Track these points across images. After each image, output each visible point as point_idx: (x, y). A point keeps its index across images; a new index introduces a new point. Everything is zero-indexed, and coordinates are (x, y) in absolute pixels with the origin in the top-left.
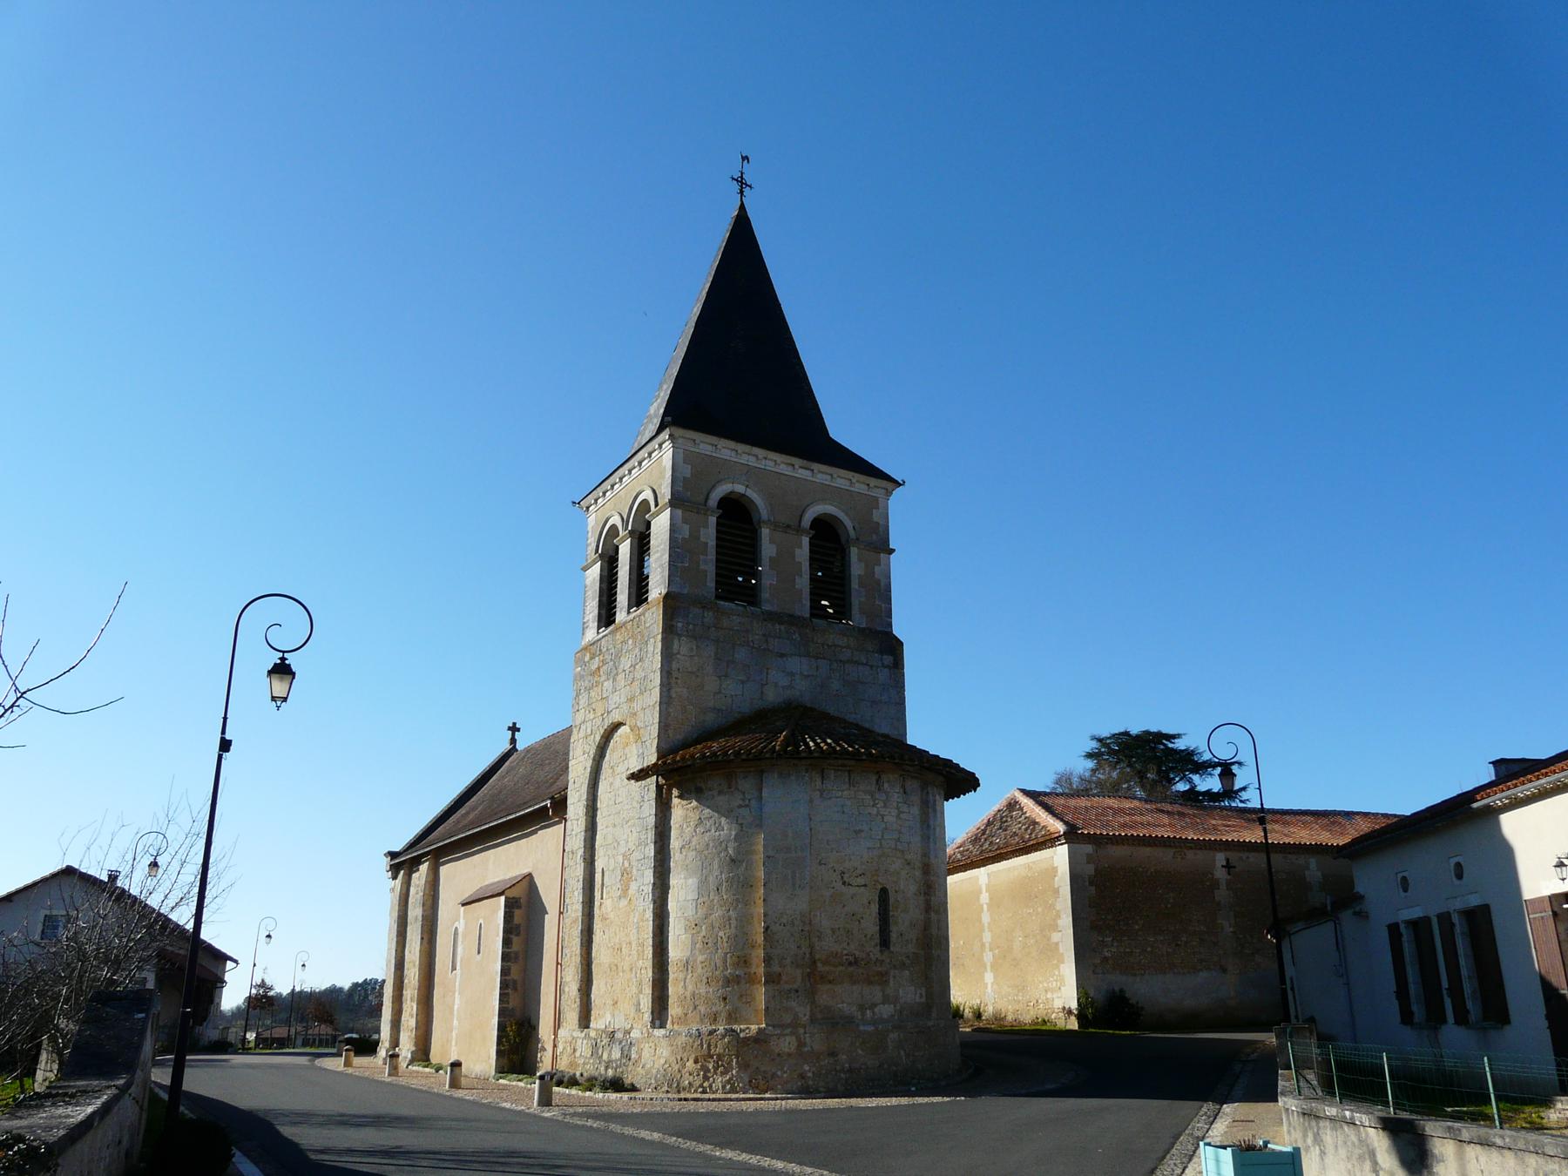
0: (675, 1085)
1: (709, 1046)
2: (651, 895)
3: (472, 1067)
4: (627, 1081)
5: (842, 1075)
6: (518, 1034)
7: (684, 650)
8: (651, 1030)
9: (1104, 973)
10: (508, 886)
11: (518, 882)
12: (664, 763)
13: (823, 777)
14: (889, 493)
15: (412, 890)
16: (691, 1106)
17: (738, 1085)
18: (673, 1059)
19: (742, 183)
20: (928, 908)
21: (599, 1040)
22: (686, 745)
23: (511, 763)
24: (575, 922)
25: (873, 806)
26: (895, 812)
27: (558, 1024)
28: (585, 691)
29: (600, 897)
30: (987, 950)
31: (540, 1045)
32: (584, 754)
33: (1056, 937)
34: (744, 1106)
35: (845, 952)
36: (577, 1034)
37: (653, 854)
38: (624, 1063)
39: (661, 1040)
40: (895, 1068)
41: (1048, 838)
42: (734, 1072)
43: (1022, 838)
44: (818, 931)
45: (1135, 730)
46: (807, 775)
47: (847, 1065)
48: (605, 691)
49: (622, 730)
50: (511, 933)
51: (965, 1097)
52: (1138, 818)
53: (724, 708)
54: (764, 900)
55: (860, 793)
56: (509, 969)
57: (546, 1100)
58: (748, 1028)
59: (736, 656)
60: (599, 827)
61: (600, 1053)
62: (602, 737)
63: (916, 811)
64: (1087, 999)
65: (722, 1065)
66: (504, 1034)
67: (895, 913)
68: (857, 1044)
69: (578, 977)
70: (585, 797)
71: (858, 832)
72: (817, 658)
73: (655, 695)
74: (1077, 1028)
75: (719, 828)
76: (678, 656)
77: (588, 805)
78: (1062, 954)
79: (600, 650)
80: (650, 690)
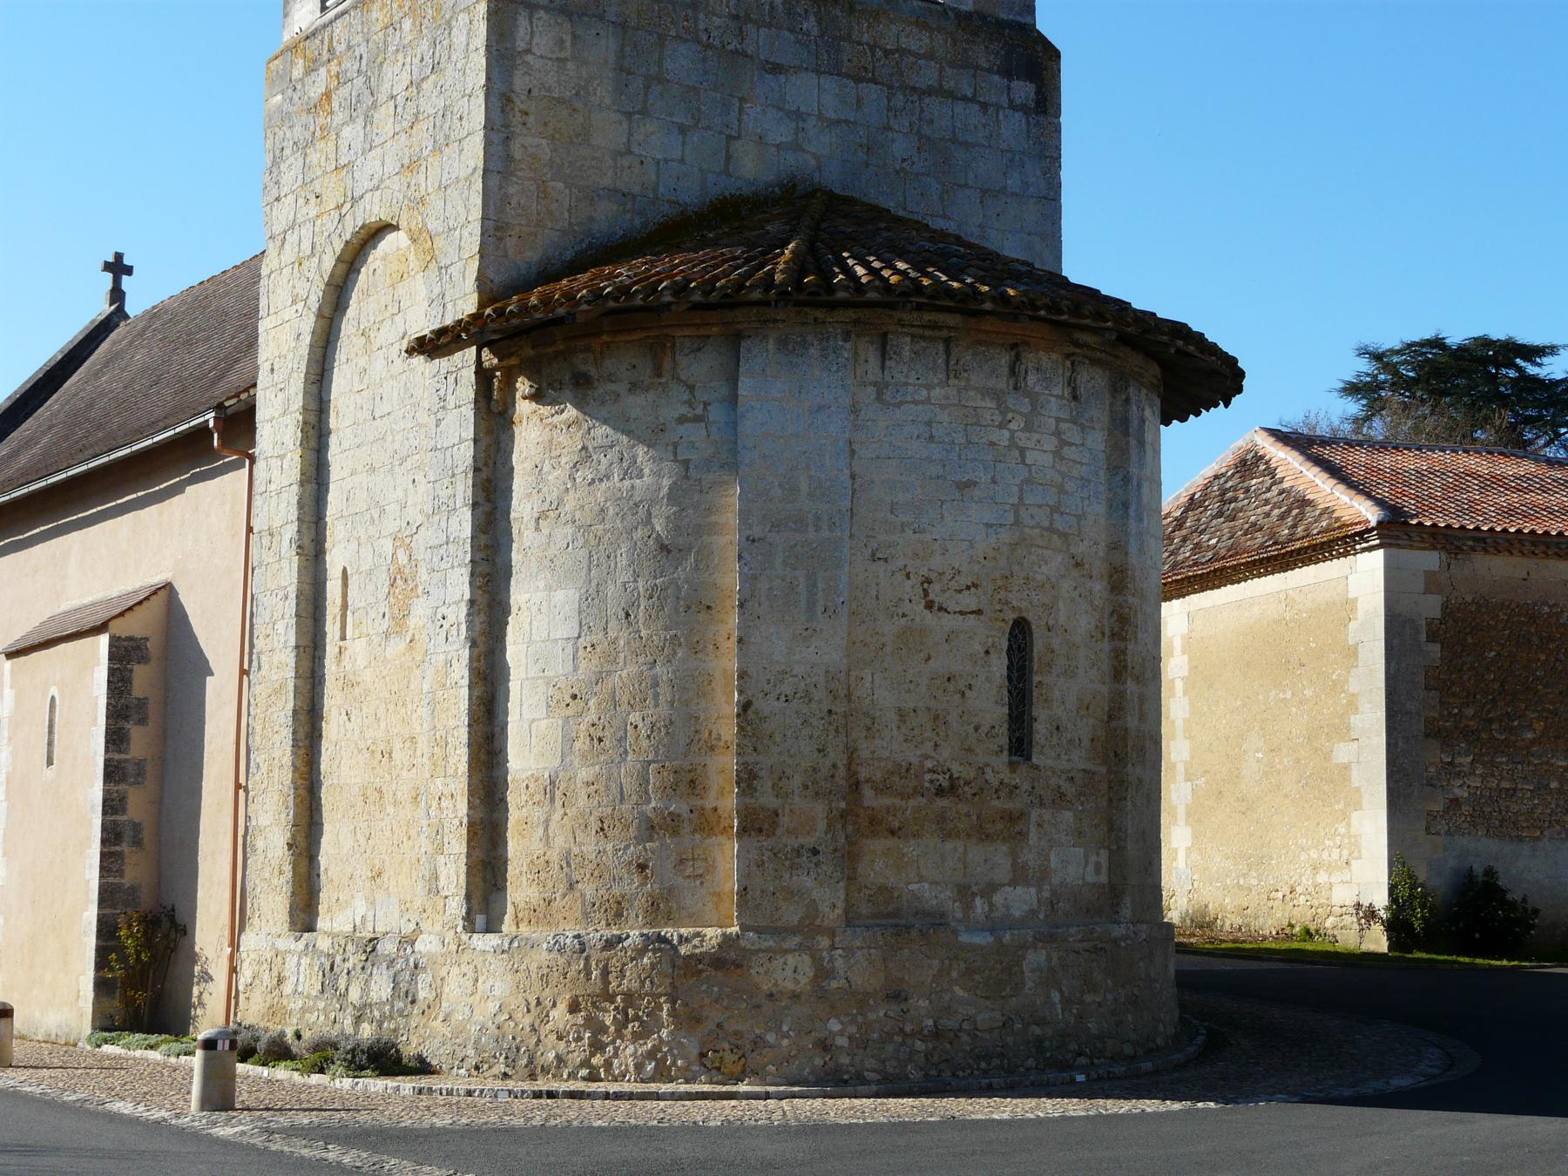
0: (524, 1062)
1: (605, 973)
2: (463, 627)
3: (37, 1014)
4: (409, 1050)
5: (919, 1045)
6: (147, 942)
7: (542, 44)
8: (465, 937)
9: (1449, 833)
10: (119, 610)
12: (500, 313)
16: (571, 1112)
17: (674, 1063)
18: (517, 1002)
20: (1119, 670)
21: (338, 959)
23: (114, 343)
25: (1001, 426)
26: (1050, 443)
28: (294, 153)
29: (338, 635)
31: (197, 969)
32: (294, 302)
33: (1343, 753)
34: (698, 1112)
35: (929, 764)
36: (288, 943)
39: (490, 957)
40: (1037, 1030)
41: (1336, 534)
42: (664, 1033)
43: (1273, 535)
44: (867, 714)
45: (1456, 335)
46: (848, 345)
47: (930, 1022)
48: (343, 149)
50: (126, 718)
51: (1217, 1102)
52: (1539, 499)
53: (636, 189)
54: (740, 641)
55: (971, 393)
56: (123, 800)
57: (219, 1097)
58: (698, 935)
59: (668, 64)
60: (335, 473)
62: (339, 260)
63: (1097, 440)
64: (1413, 887)
65: (637, 1018)
68: (954, 974)
70: (298, 403)
72: (858, 80)
73: (474, 152)
74: (1385, 950)
75: (631, 470)
76: (529, 58)
77: (305, 423)
78: (1358, 790)
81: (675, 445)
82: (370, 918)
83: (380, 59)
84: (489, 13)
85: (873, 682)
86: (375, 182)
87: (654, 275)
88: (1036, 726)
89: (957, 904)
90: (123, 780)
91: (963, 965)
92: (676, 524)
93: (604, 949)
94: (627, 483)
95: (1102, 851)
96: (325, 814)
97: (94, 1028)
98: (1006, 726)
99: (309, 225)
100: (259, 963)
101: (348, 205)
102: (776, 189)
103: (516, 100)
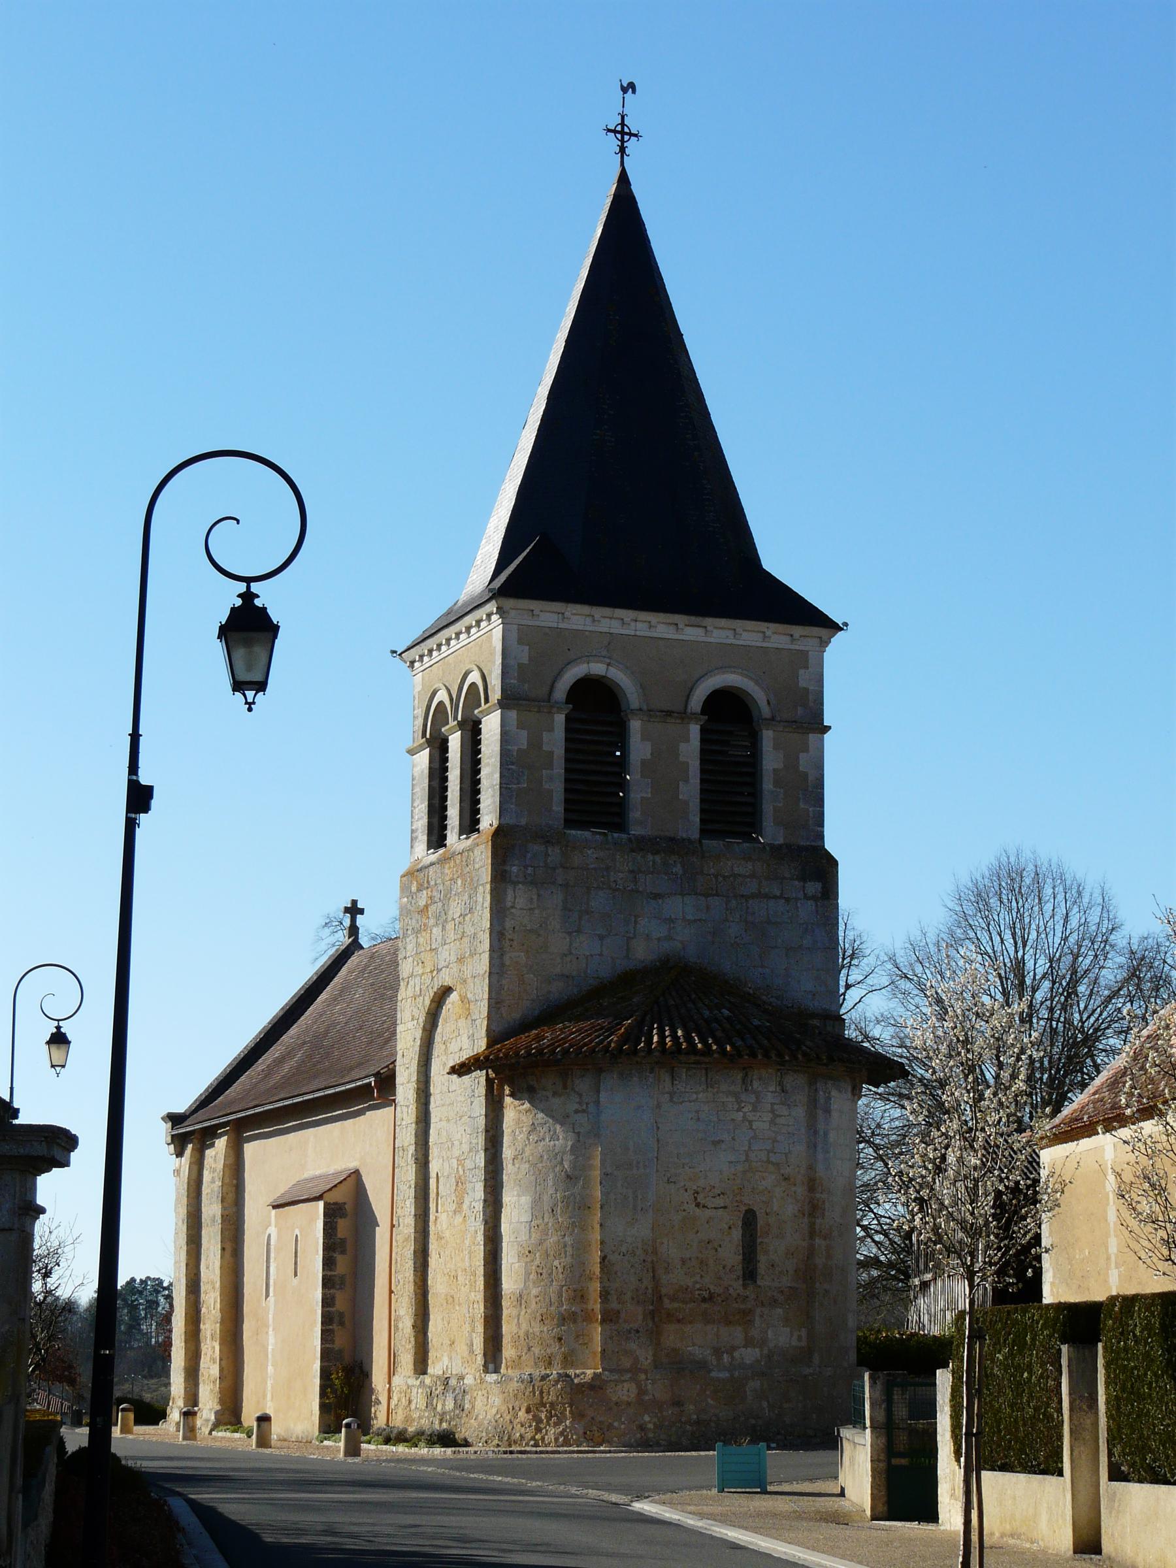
0: (506, 1438)
1: (541, 1393)
3: (292, 1425)
7: (521, 902)
8: (483, 1376)
11: (341, 1182)
13: (673, 1077)
14: (824, 643)
15: (207, 1176)
18: (504, 1408)
19: (623, 133)
21: (434, 1388)
22: (524, 1026)
24: (406, 1240)
25: (739, 1110)
26: (768, 1117)
27: (391, 1373)
30: (1113, 1265)
31: (374, 1397)
32: (413, 1020)
35: (698, 1286)
36: (413, 1381)
37: (483, 1164)
38: (458, 1415)
40: (753, 1422)
42: (568, 1422)
46: (651, 1075)
47: (695, 1417)
49: (454, 997)
50: (334, 1251)
53: (574, 973)
56: (333, 1298)
58: (583, 1373)
60: (434, 1119)
61: (435, 1404)
62: (432, 1001)
63: (800, 1112)
66: (328, 1383)
67: (766, 1240)
69: (411, 1311)
70: (414, 1078)
71: (716, 1143)
72: (706, 896)
75: (554, 1137)
76: (513, 910)
77: (418, 1089)
79: (428, 882)
80: (480, 954)
81: (573, 1124)
82: (450, 1367)
83: (448, 896)
84: (492, 890)
85: (668, 1245)
86: (447, 963)
87: (560, 1040)
88: (759, 1265)
89: (714, 1357)
90: (333, 1287)
91: (712, 1388)
92: (574, 1166)
93: (541, 1381)
94: (552, 1143)
95: (803, 1329)
96: (431, 1309)
97: (320, 1432)
98: (741, 1266)
99: (419, 978)
100: (401, 1393)
101: (435, 972)
102: (658, 963)
103: (506, 934)
